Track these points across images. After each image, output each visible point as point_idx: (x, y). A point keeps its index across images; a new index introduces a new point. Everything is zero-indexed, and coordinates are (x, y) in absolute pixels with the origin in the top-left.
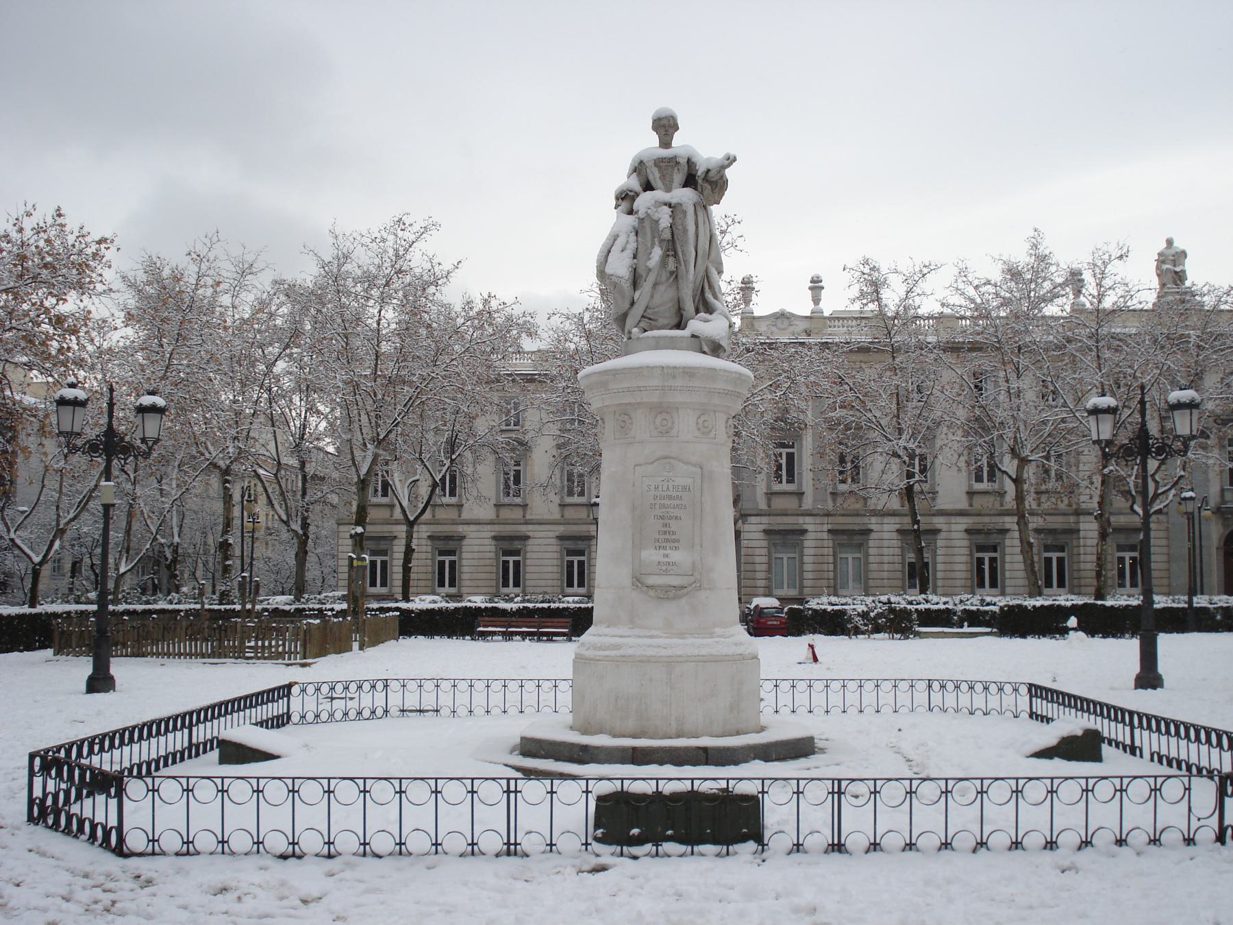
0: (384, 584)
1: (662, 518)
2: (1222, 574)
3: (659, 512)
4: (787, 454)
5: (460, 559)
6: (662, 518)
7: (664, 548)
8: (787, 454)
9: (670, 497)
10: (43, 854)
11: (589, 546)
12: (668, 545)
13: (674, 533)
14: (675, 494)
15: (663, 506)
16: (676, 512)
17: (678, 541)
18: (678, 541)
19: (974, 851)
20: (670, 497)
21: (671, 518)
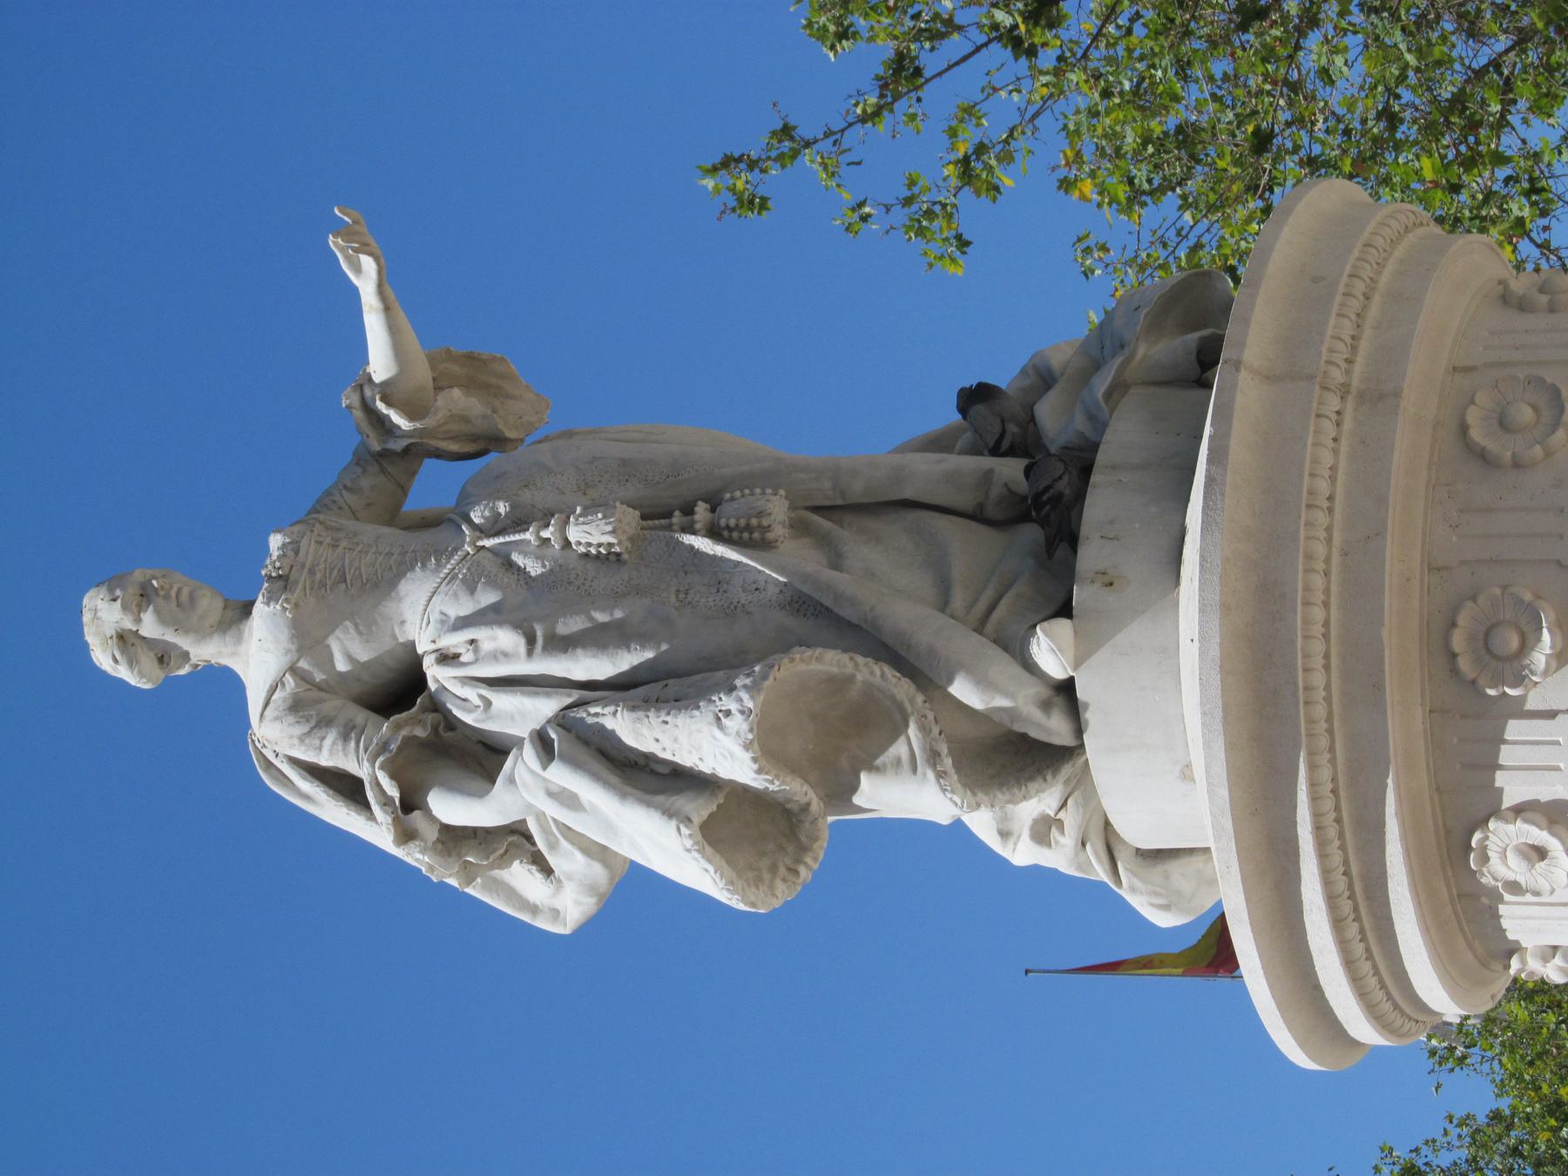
19: (719, 219)
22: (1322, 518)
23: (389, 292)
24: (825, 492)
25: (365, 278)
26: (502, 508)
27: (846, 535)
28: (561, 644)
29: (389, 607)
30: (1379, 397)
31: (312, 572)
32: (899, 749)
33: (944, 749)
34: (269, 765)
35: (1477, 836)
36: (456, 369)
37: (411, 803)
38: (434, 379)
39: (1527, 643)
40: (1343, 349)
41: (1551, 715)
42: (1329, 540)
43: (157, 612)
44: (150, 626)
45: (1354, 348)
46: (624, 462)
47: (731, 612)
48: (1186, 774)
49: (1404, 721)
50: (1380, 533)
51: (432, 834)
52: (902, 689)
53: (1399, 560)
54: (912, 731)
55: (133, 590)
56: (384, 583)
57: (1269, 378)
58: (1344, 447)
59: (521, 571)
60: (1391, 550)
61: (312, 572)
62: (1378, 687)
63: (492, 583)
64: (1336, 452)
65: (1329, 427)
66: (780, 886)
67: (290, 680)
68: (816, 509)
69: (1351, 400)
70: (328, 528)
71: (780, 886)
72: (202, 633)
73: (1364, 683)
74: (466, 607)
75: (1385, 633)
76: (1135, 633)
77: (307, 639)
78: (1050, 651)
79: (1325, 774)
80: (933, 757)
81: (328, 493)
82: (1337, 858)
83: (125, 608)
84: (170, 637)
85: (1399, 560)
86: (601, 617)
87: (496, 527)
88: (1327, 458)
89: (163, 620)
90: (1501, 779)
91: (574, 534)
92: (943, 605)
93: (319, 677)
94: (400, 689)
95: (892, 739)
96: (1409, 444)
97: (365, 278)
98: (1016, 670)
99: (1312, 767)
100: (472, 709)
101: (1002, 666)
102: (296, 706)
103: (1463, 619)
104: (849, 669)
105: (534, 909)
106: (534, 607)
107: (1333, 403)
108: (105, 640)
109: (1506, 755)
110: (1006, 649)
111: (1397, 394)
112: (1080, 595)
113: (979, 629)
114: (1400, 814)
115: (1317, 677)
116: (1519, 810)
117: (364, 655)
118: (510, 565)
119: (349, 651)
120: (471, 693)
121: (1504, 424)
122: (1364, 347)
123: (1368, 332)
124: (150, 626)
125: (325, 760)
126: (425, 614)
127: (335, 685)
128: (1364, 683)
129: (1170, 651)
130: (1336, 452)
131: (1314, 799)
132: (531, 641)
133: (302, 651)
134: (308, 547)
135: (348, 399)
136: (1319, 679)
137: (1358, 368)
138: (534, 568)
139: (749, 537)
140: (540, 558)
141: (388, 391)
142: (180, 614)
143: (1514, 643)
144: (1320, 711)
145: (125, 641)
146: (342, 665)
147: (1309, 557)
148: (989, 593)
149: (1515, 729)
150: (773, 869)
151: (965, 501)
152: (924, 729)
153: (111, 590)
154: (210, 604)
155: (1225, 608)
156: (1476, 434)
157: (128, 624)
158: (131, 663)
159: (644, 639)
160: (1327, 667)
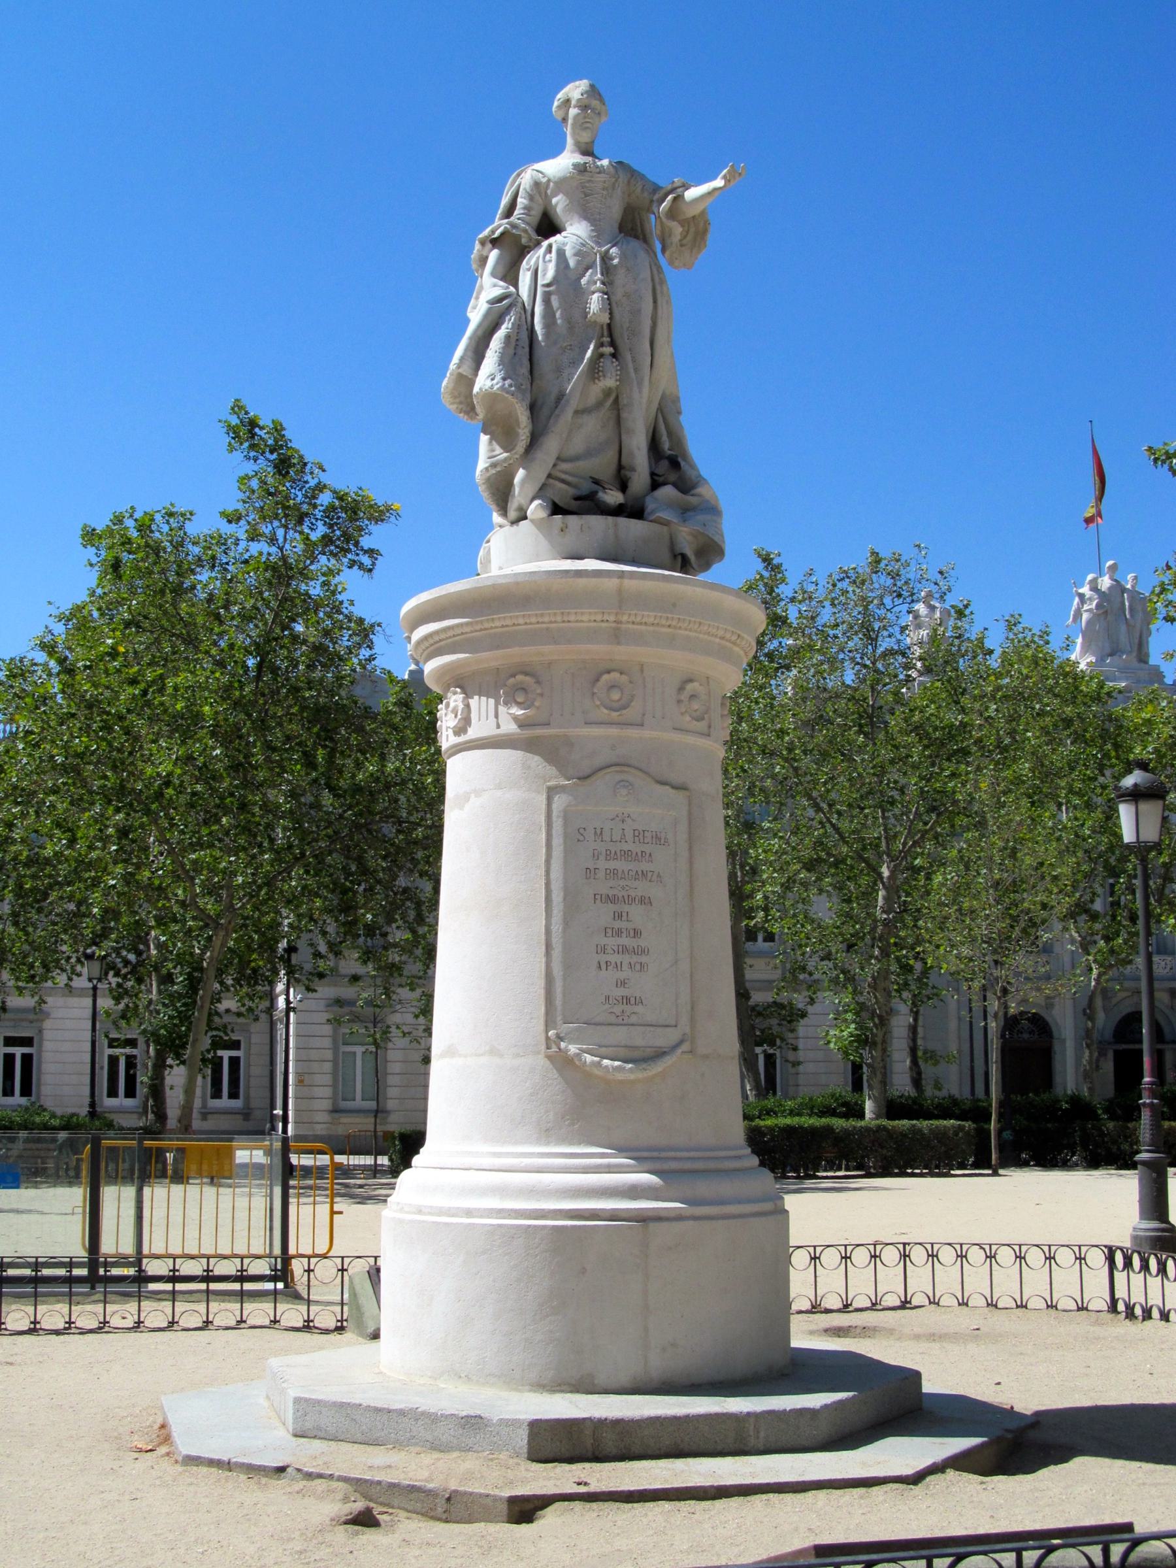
0: (234, 1095)
1: (611, 899)
2: (1000, 1076)
3: (604, 888)
4: (231, 1058)
5: (40, 1051)
6: (611, 899)
7: (618, 966)
8: (231, 1058)
9: (626, 854)
10: (11, 1364)
11: (40, 1031)
12: (626, 959)
13: (637, 933)
14: (636, 848)
15: (613, 874)
16: (641, 888)
17: (644, 951)
18: (644, 951)
19: (246, 431)
20: (626, 854)
21: (630, 900)
22: (559, 619)
23: (717, 194)
24: (624, 400)
25: (719, 183)
26: (616, 261)
27: (605, 411)
28: (547, 301)
29: (576, 218)
30: (617, 636)
31: (589, 181)
32: (498, 450)
33: (499, 469)
34: (519, 175)
35: (458, 690)
36: (702, 225)
37: (495, 242)
38: (694, 217)
39: (519, 705)
40: (638, 619)
41: (497, 716)
42: (551, 622)
43: (578, 115)
44: (573, 112)
45: (641, 624)
46: (639, 311)
47: (559, 370)
48: (501, 568)
49: (490, 659)
50: (556, 643)
51: (485, 254)
52: (521, 446)
53: (549, 651)
54: (505, 455)
55: (586, 102)
56: (586, 214)
57: (620, 591)
58: (593, 624)
59: (583, 275)
60: (552, 647)
61: (589, 181)
62: (498, 647)
63: (578, 263)
64: (590, 621)
65: (599, 618)
66: (455, 406)
67: (544, 180)
68: (617, 398)
69: (614, 625)
70: (614, 184)
71: (455, 406)
72: (574, 134)
73: (498, 642)
74: (569, 253)
75: (517, 649)
76: (544, 543)
77: (562, 184)
78: (536, 509)
79: (468, 629)
80: (494, 465)
81: (643, 177)
82: (443, 636)
83: (579, 100)
84: (570, 121)
85: (549, 651)
86: (558, 315)
87: (606, 258)
88: (585, 618)
89: (576, 117)
90: (476, 697)
91: (595, 296)
92: (559, 459)
93: (549, 192)
94: (548, 227)
95: (502, 447)
96: (599, 650)
97: (719, 183)
98: (530, 496)
99: (467, 624)
100: (528, 263)
101: (532, 489)
102: (537, 184)
103: (528, 679)
104: (522, 426)
105: (477, 298)
106: (567, 281)
107: (612, 618)
108: (567, 94)
109: (484, 699)
110: (540, 489)
111: (619, 643)
112: (558, 518)
113: (549, 476)
114: (459, 660)
115: (498, 622)
116: (468, 706)
117: (559, 210)
118: (587, 270)
119: (559, 202)
120: (534, 259)
121: (612, 687)
122: (643, 628)
123: (651, 628)
124: (573, 112)
125: (519, 200)
126: (574, 233)
127: (547, 199)
128: (498, 642)
129: (538, 558)
130: (590, 621)
131: (457, 625)
132: (548, 285)
133: (556, 183)
134: (601, 178)
135: (677, 181)
136: (497, 624)
137: (630, 626)
138: (584, 281)
139: (595, 370)
140: (588, 282)
141: (678, 198)
142: (580, 125)
143: (519, 700)
144: (486, 625)
145: (567, 101)
146: (554, 201)
147: (542, 615)
148: (570, 479)
149: (492, 701)
150: (461, 403)
151: (624, 461)
152: (506, 459)
153: (586, 92)
154: (585, 137)
155: (517, 583)
156: (605, 677)
157: (573, 102)
158: (559, 107)
159: (547, 335)
160: (503, 626)
